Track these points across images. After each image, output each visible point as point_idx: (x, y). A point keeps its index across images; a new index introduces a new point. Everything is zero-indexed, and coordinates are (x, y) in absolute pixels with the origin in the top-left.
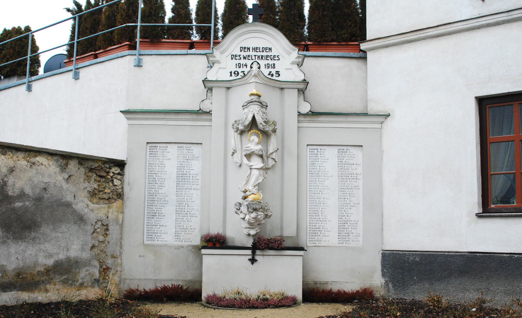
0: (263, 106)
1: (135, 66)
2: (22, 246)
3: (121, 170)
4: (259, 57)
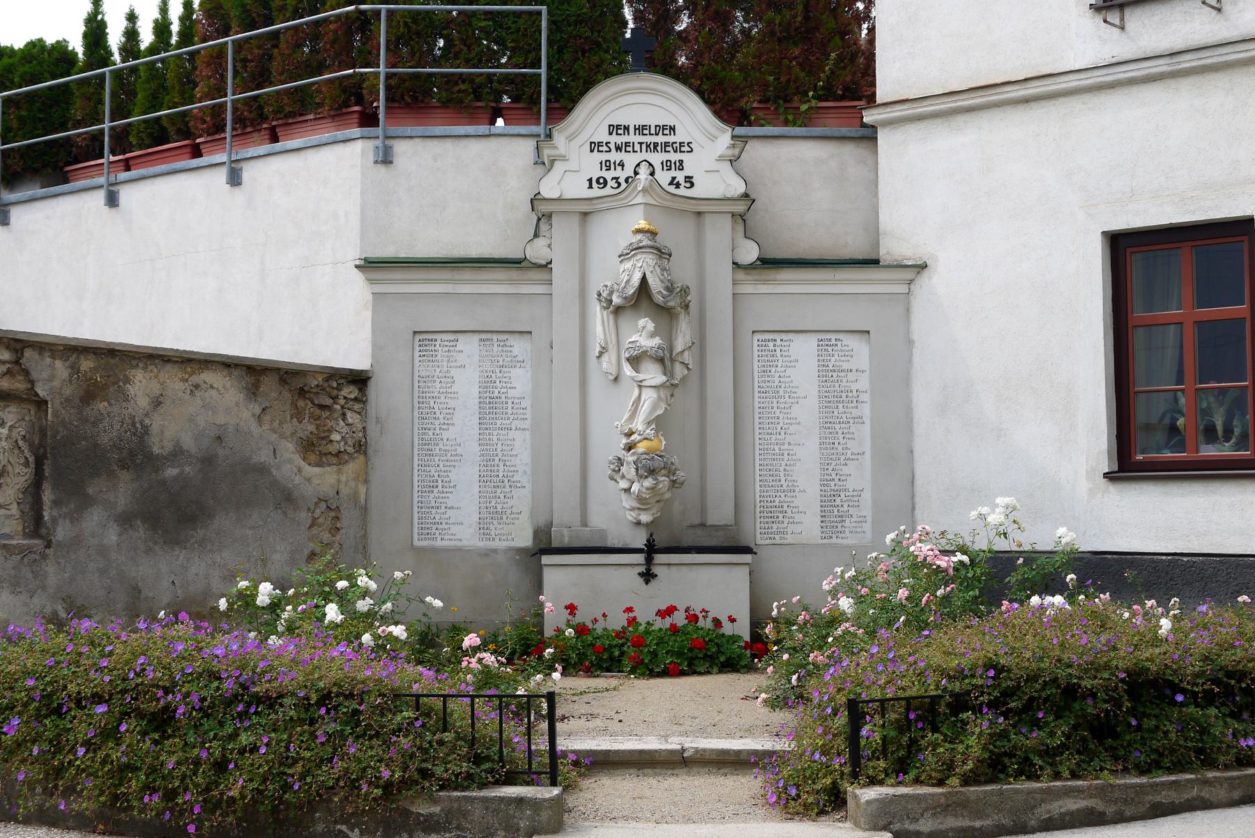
1: (376, 162)
2: (181, 555)
3: (360, 390)
4: (648, 146)
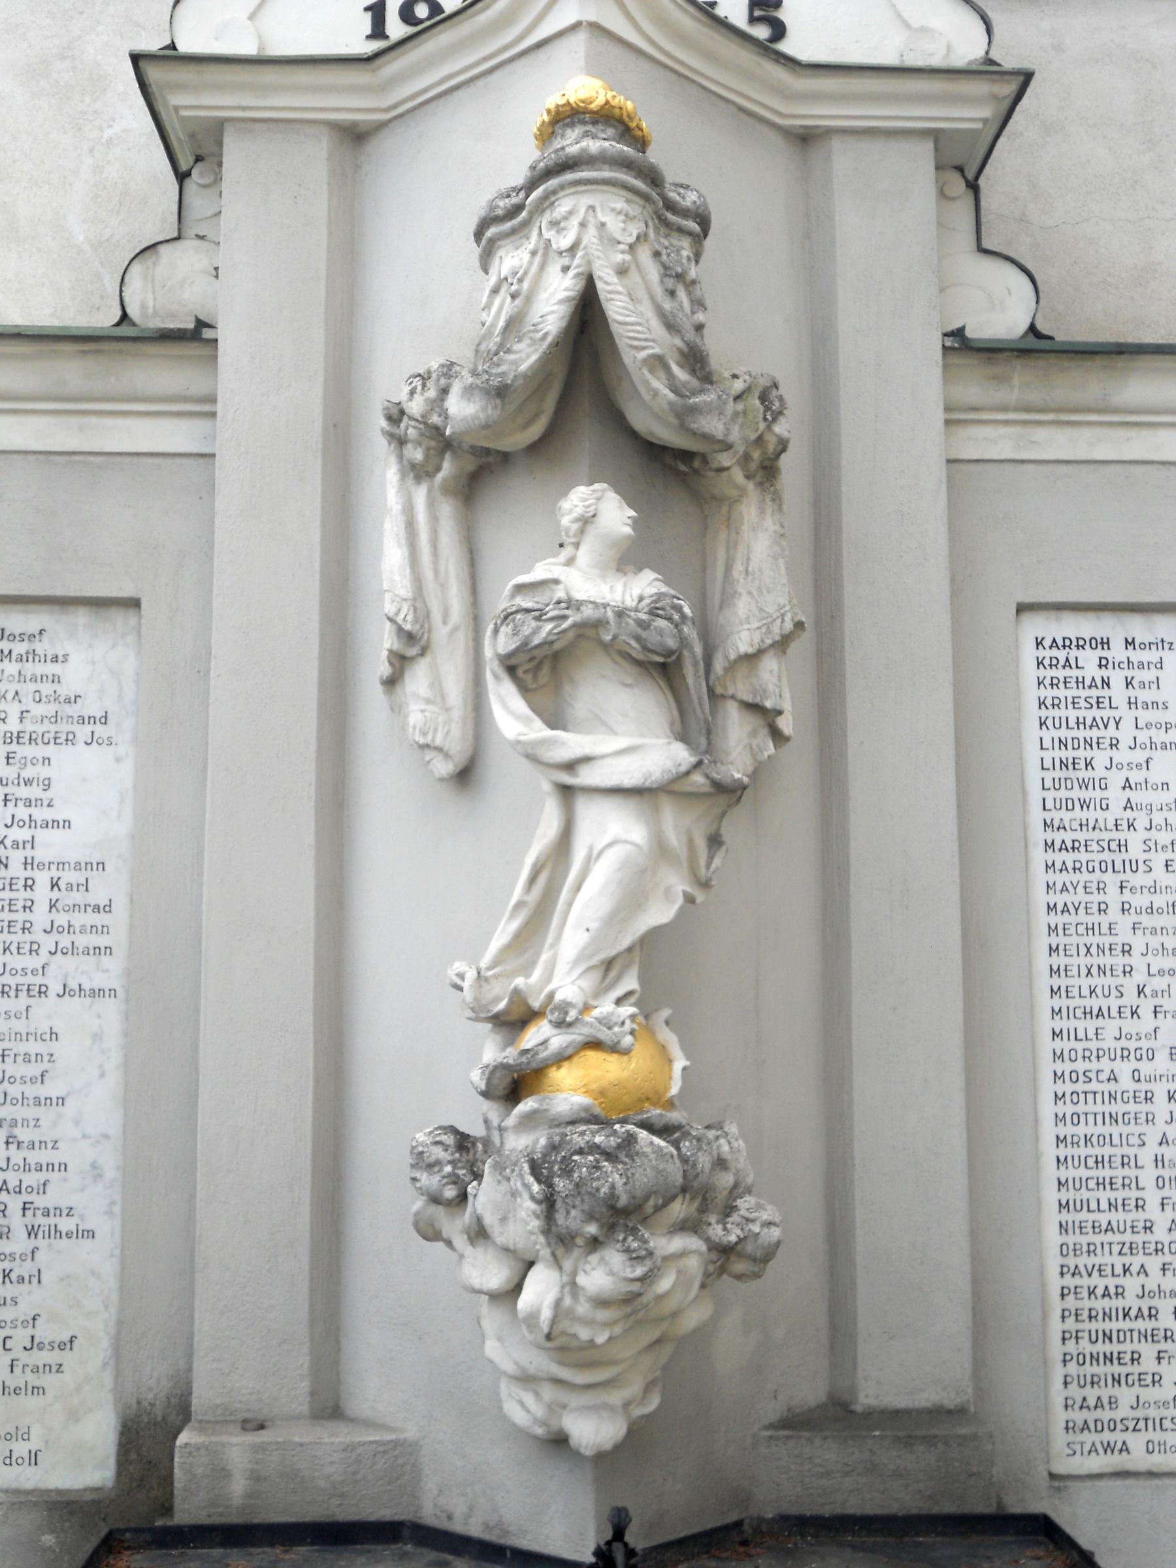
0: (676, 220)
